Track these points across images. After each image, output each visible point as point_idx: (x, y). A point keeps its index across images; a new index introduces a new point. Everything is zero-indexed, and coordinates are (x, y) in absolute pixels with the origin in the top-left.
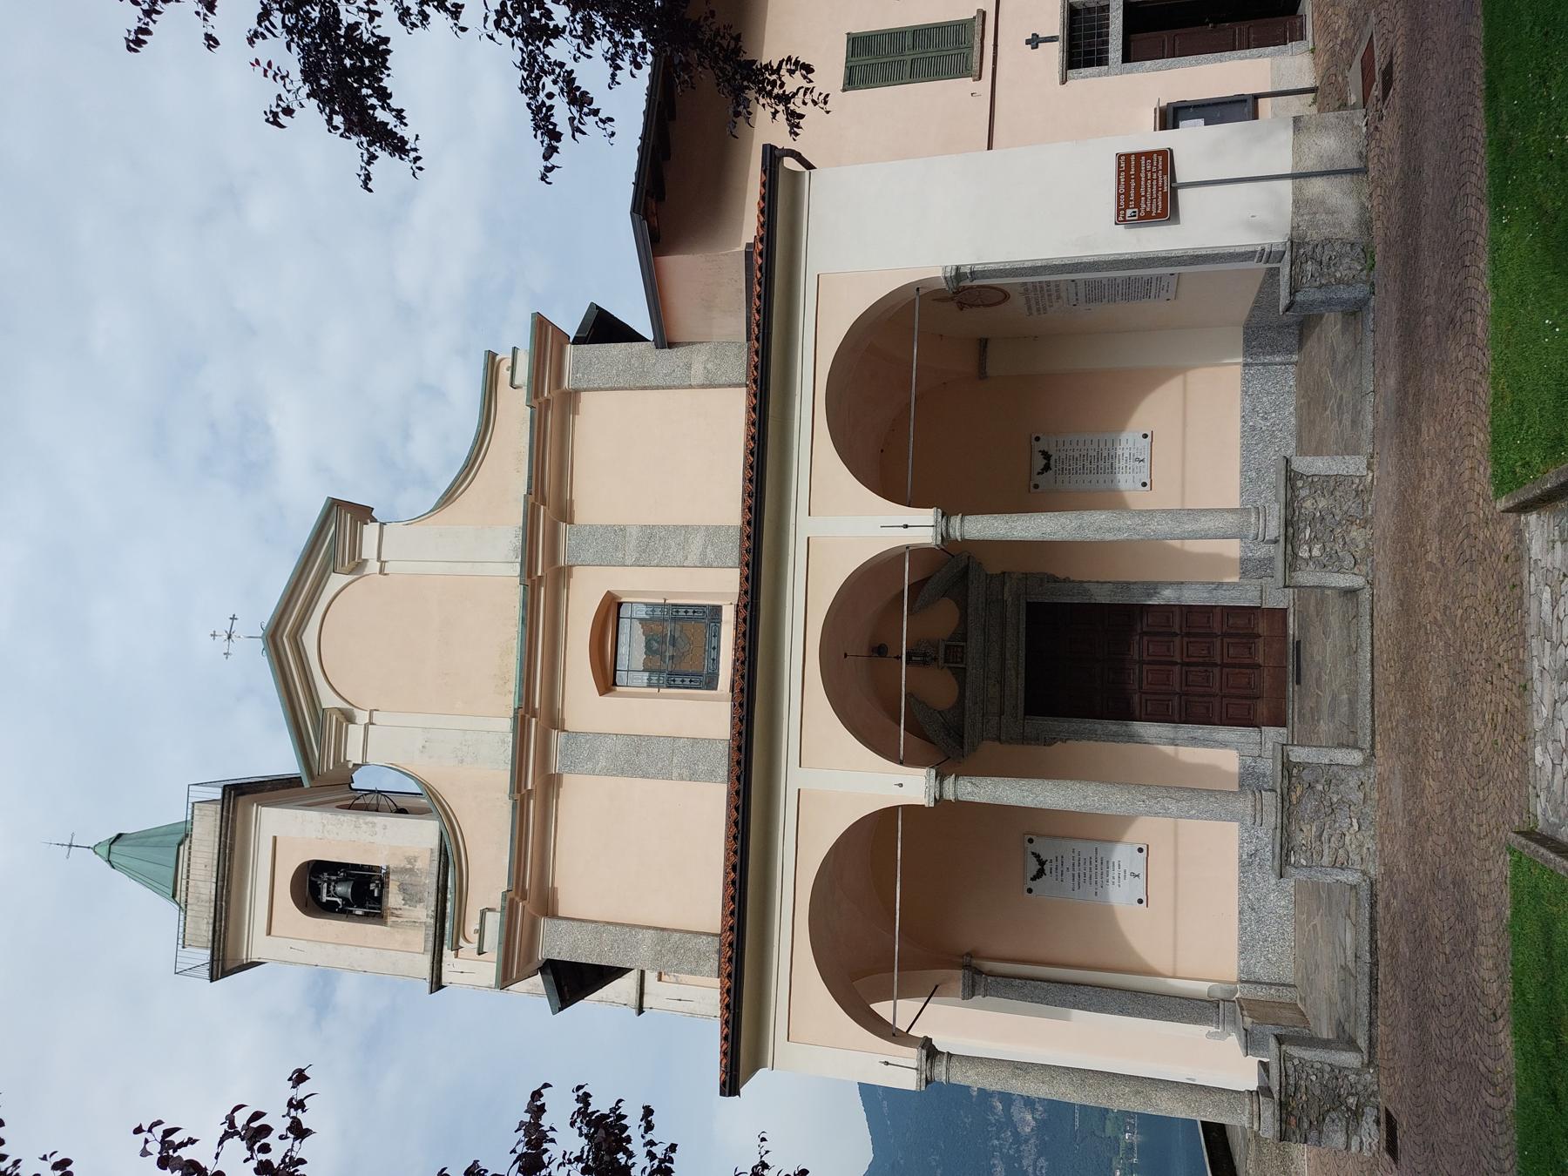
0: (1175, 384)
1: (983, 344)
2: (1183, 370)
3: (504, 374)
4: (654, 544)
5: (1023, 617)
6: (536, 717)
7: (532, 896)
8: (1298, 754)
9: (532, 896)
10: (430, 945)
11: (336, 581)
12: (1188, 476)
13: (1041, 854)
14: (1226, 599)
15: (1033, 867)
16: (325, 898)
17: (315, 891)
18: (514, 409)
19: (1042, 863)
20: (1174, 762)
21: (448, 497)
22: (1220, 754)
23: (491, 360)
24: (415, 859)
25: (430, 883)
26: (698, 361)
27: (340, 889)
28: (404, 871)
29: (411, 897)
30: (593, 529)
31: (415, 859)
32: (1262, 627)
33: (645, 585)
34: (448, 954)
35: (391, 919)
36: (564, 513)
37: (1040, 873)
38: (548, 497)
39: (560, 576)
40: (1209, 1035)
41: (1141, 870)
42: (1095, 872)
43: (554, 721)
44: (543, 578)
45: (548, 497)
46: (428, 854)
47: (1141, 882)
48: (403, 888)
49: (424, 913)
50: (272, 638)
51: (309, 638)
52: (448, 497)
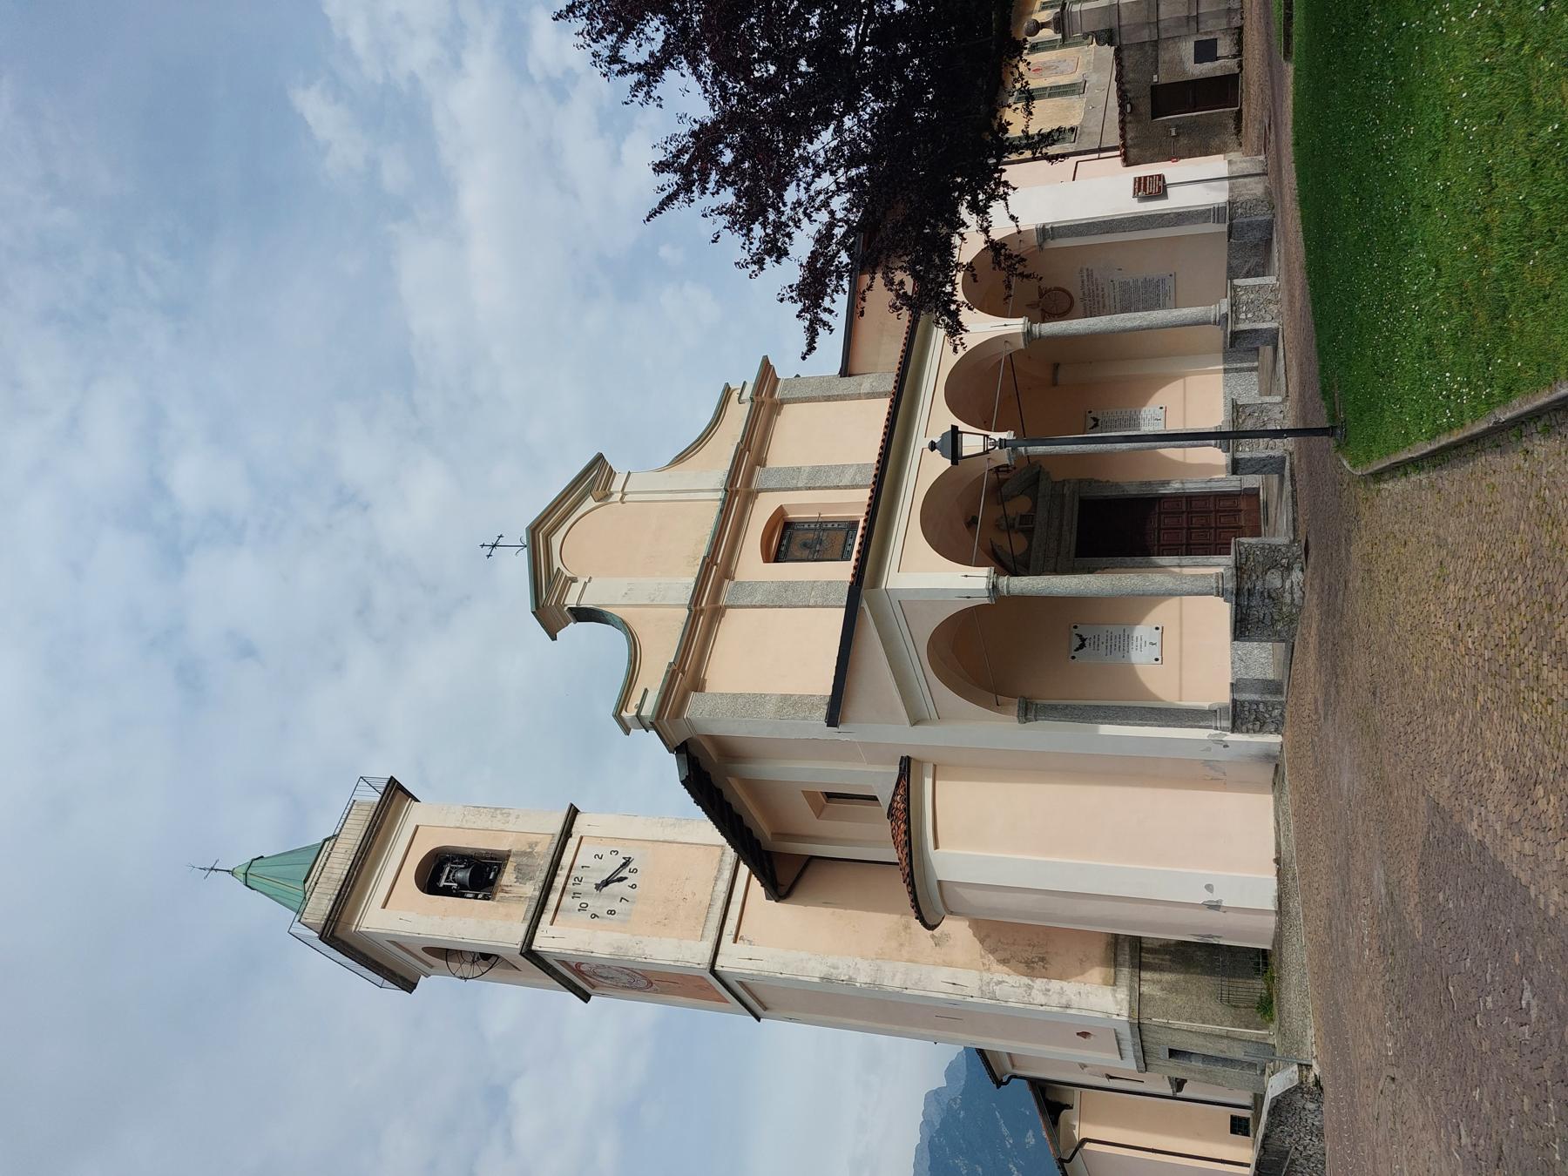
0: (1180, 382)
1: (1056, 366)
2: (1183, 376)
3: (735, 396)
4: (817, 479)
5: (1076, 508)
6: (716, 568)
7: (687, 674)
8: (1240, 455)
9: (689, 674)
10: (530, 914)
11: (590, 503)
12: (1189, 413)
13: (1084, 633)
14: (1217, 487)
15: (1078, 642)
16: (443, 883)
17: (436, 876)
18: (738, 414)
19: (1083, 640)
20: (1163, 457)
21: (680, 459)
22: (1217, 567)
23: (727, 392)
24: (537, 844)
25: (545, 864)
26: (866, 384)
27: (459, 875)
28: (524, 854)
29: (523, 875)
30: (779, 470)
31: (537, 844)
32: (1243, 505)
33: (805, 504)
34: (546, 917)
35: (499, 895)
36: (761, 461)
37: (1082, 646)
38: (752, 450)
39: (750, 496)
40: (1166, 483)
41: (1157, 640)
42: (1121, 643)
43: (727, 574)
44: (737, 494)
45: (752, 450)
46: (548, 839)
47: (1157, 649)
48: (518, 869)
49: (531, 890)
50: (533, 530)
51: (556, 541)
52: (680, 459)
